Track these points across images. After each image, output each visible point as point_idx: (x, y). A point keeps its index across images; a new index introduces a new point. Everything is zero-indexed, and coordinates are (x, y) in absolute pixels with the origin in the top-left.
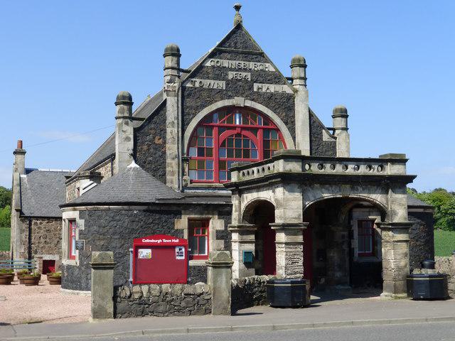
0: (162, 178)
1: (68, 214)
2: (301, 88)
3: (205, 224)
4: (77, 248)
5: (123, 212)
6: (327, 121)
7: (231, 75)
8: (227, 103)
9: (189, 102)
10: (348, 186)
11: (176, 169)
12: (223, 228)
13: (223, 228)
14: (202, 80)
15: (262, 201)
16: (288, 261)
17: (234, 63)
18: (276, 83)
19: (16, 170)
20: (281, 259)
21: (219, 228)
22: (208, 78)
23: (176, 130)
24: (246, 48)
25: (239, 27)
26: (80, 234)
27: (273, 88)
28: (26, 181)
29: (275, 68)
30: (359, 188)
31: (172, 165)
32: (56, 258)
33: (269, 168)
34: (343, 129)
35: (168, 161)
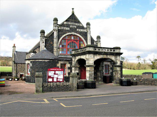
0: (53, 52)
1: (27, 62)
3: (65, 64)
4: (30, 71)
6: (95, 39)
7: (71, 26)
8: (70, 33)
9: (60, 33)
11: (56, 50)
14: (64, 28)
16: (89, 75)
17: (72, 23)
18: (83, 29)
19: (13, 52)
20: (88, 74)
22: (65, 27)
25: (73, 14)
26: (31, 68)
27: (82, 30)
28: (16, 54)
29: (82, 25)
31: (55, 49)
32: (23, 74)
33: (84, 50)
34: (99, 41)
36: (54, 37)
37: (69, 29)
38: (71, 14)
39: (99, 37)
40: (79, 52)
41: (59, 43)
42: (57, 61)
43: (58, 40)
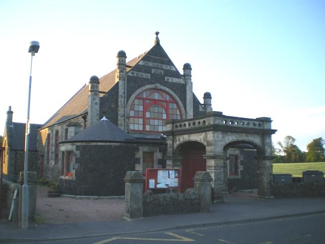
3: (151, 154)
4: (74, 169)
6: (202, 101)
10: (244, 134)
12: (161, 158)
13: (161, 158)
14: (138, 73)
15: (188, 142)
17: (156, 64)
18: (177, 77)
21: (160, 158)
27: (175, 80)
29: (176, 69)
35: (119, 118)
37: (149, 76)
39: (207, 96)
40: (183, 128)
41: (129, 107)
42: (135, 145)
43: (128, 100)
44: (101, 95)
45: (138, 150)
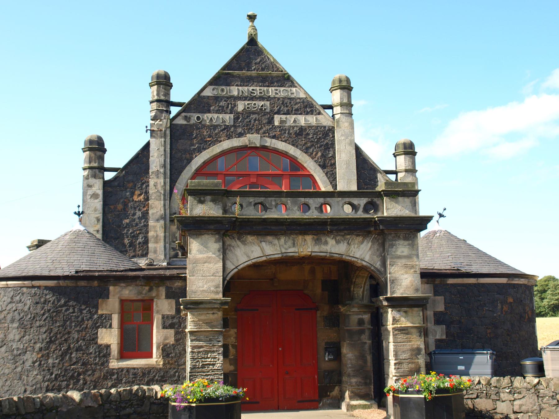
2: (344, 119)
3: (147, 306)
5: (25, 290)
7: (241, 106)
9: (182, 144)
10: (309, 238)
13: (173, 312)
17: (245, 89)
23: (162, 181)
24: (263, 69)
25: (252, 41)
27: (302, 120)
29: (306, 93)
30: (329, 240)
35: (151, 223)
36: (149, 169)
37: (228, 118)
38: (245, 40)
42: (96, 283)
44: (109, 176)
45: (105, 295)
